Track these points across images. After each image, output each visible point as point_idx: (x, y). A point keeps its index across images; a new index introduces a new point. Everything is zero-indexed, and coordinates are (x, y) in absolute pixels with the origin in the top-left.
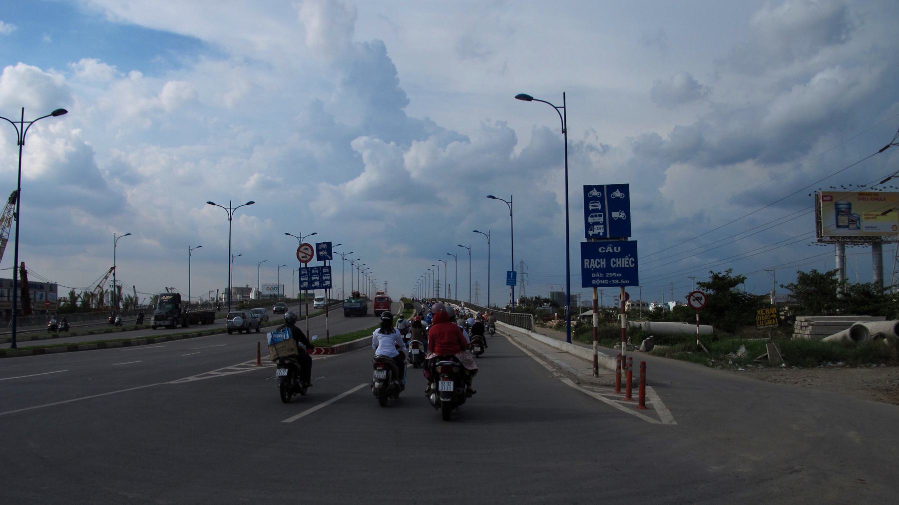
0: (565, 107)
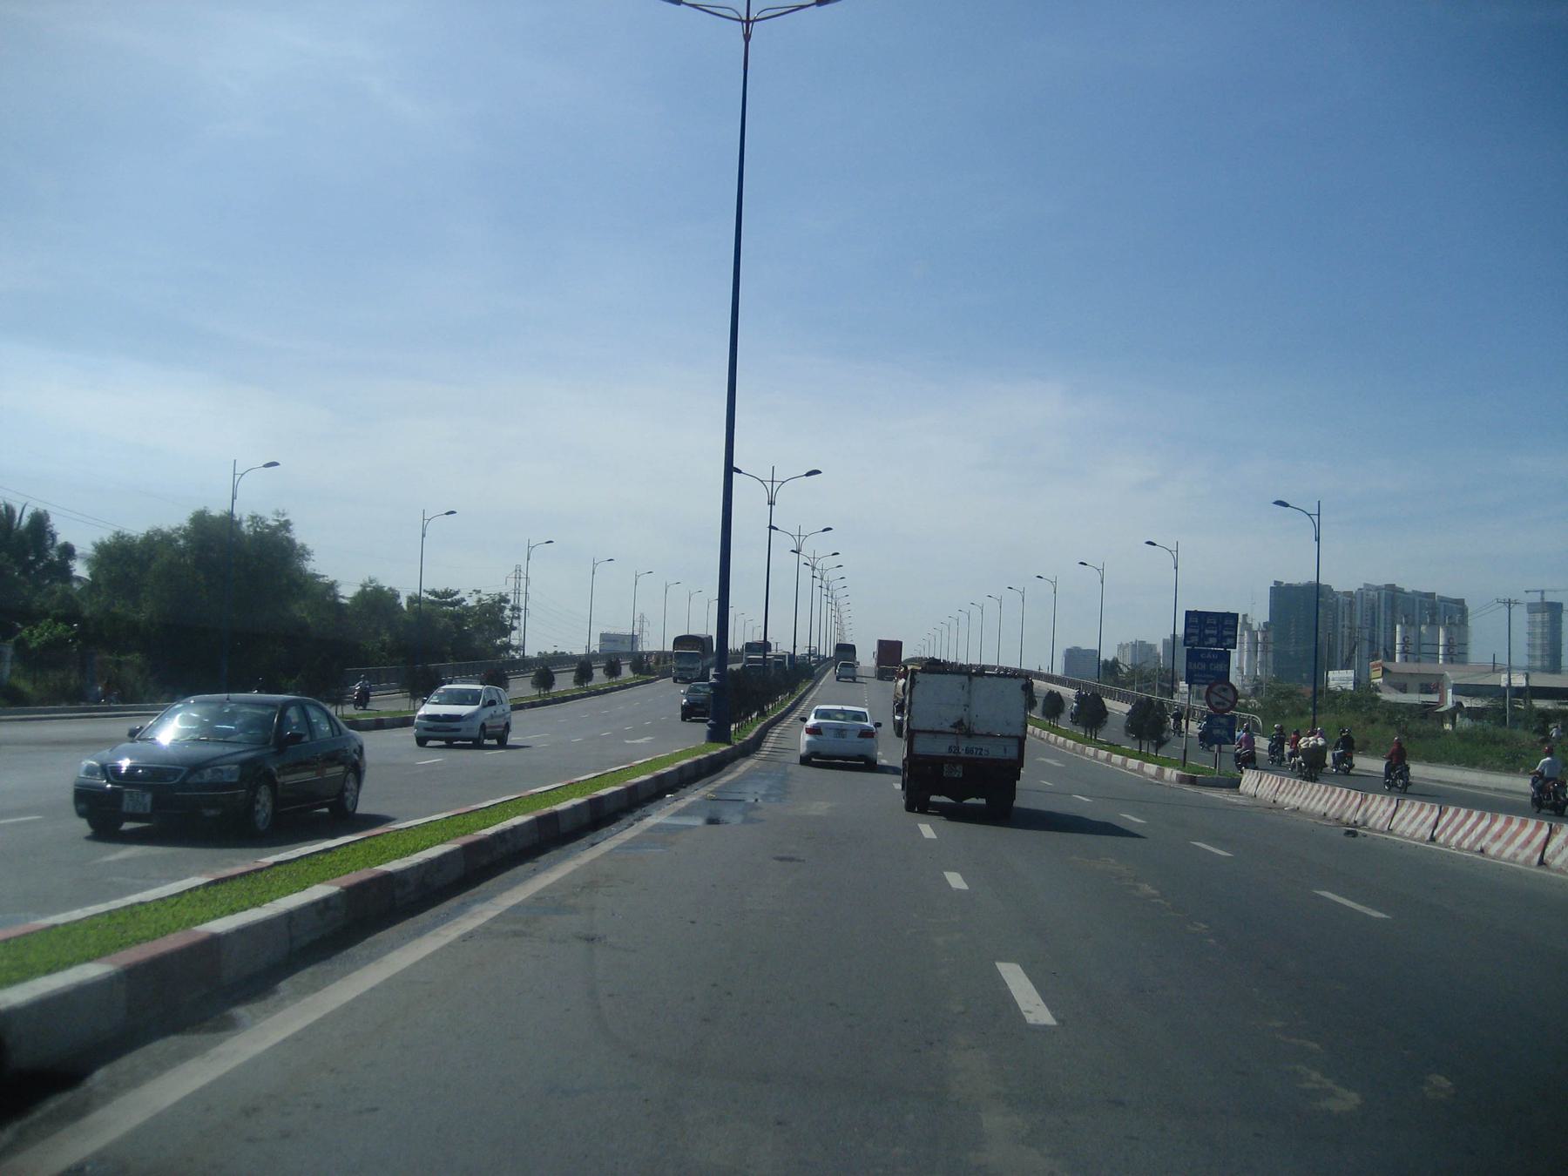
0: (1319, 515)
